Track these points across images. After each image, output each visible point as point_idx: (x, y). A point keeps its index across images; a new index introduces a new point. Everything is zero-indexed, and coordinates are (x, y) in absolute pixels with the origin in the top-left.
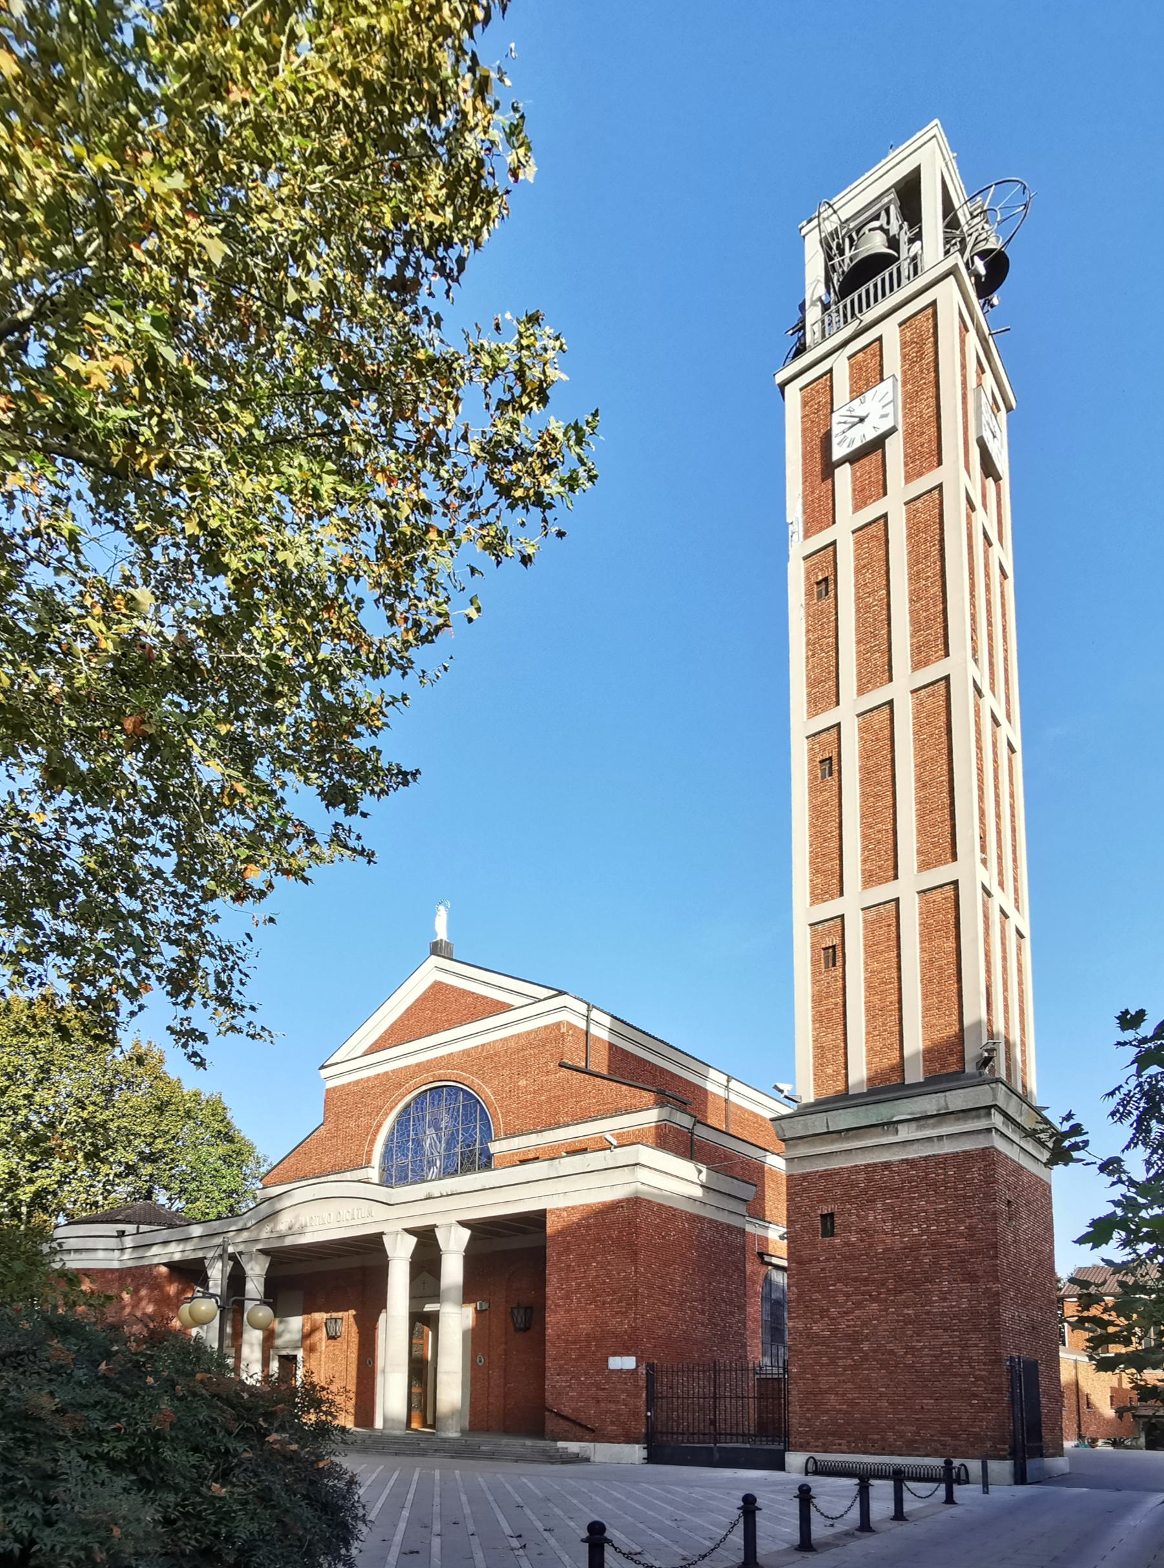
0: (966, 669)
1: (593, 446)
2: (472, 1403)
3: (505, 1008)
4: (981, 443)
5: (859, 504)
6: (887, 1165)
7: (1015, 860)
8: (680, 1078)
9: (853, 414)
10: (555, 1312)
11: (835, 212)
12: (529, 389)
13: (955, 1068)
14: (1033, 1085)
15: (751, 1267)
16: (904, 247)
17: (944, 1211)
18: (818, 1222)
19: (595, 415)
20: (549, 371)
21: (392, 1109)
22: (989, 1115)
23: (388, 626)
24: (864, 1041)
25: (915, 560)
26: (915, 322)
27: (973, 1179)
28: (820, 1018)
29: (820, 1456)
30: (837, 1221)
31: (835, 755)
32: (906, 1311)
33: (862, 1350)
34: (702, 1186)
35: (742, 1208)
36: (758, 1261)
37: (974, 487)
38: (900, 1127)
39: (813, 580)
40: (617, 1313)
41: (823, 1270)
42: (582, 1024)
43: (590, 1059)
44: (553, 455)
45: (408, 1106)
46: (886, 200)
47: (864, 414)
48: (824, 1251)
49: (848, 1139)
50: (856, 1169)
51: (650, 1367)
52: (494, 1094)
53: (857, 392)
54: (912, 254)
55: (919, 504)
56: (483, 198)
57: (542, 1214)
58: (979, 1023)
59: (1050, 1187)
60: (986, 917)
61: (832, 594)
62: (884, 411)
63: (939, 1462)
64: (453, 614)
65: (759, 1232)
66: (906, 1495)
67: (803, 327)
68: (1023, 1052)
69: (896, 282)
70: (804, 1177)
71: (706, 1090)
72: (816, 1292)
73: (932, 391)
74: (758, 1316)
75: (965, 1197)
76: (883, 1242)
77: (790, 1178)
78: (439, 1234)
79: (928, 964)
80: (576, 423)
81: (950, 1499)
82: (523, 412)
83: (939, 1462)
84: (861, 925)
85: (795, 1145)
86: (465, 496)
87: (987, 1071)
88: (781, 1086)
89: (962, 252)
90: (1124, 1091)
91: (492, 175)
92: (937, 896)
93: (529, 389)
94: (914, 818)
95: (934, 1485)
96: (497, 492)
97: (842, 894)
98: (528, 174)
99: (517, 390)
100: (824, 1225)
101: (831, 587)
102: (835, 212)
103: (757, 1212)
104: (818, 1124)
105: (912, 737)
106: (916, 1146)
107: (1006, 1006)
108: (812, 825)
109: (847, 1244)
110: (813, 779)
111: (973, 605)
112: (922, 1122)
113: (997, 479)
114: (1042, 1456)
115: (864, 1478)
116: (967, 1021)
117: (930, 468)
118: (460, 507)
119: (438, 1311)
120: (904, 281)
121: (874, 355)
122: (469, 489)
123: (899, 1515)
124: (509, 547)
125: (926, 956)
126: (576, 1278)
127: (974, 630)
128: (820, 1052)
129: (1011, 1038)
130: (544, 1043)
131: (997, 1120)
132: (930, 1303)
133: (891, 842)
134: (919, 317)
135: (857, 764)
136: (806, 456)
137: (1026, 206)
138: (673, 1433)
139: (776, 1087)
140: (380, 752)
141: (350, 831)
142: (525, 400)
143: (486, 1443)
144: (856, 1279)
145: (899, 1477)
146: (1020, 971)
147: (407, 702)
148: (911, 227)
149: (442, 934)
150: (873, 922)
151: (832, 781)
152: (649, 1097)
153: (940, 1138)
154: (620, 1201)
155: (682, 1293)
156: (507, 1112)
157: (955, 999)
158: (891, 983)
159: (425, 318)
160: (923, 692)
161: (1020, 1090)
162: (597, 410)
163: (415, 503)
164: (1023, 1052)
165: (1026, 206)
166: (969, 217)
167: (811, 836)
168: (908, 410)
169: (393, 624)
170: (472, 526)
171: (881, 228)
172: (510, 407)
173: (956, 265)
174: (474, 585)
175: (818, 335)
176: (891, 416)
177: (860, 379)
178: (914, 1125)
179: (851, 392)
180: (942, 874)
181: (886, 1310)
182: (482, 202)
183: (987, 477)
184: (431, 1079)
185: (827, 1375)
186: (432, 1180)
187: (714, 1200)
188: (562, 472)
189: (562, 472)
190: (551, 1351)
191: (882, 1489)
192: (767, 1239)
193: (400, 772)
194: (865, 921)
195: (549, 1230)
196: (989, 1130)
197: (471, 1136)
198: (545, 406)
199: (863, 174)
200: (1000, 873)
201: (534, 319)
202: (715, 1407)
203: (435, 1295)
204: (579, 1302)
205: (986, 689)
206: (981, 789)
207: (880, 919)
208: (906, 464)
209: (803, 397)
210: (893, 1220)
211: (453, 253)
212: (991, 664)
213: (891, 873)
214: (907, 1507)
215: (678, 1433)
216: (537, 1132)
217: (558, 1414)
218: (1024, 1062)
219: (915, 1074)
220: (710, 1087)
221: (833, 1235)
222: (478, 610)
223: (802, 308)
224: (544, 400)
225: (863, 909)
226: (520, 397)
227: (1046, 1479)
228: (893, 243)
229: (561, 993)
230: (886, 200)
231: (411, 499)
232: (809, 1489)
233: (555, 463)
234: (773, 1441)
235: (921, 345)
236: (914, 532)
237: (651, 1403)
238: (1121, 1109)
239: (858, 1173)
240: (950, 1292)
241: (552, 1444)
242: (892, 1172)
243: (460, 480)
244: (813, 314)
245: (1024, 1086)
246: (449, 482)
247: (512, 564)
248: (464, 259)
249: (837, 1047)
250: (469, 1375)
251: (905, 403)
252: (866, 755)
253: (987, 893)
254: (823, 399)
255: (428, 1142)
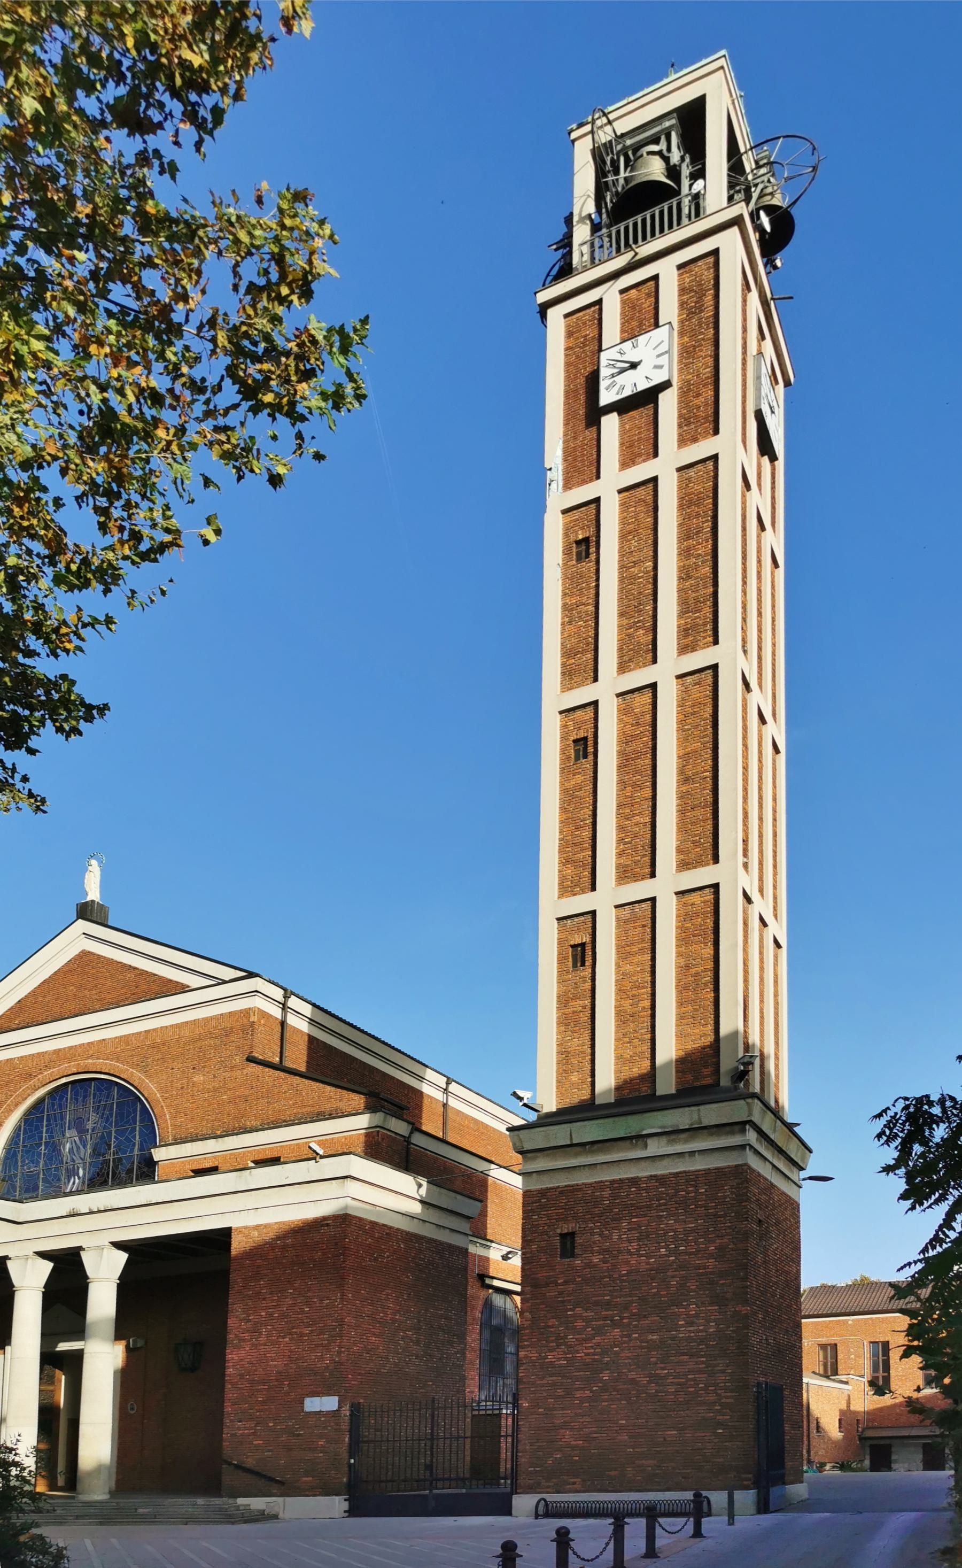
0: (735, 659)
1: (360, 361)
2: (118, 1457)
3: (183, 989)
4: (759, 416)
5: (627, 461)
6: (634, 1181)
7: (775, 866)
8: (393, 1078)
9: (624, 358)
10: (238, 1347)
11: (610, 122)
12: (290, 278)
13: (708, 1081)
14: (785, 1100)
15: (473, 1289)
16: (685, 183)
17: (693, 1230)
18: (557, 1241)
19: (365, 321)
20: (316, 262)
21: (17, 1105)
22: (743, 1131)
23: (99, 534)
24: (613, 1047)
25: (686, 534)
26: (695, 268)
27: (725, 1197)
28: (566, 1021)
29: (551, 1498)
30: (579, 1240)
31: (591, 736)
32: (650, 1337)
33: (601, 1380)
34: (421, 1202)
35: (465, 1226)
36: (478, 1284)
37: (751, 465)
38: (650, 1141)
39: (573, 538)
40: (317, 1346)
41: (561, 1293)
42: (277, 1012)
43: (286, 1053)
44: (312, 361)
45: (40, 1101)
46: (667, 124)
47: (636, 360)
48: (562, 1273)
49: (592, 1152)
50: (600, 1185)
51: (356, 1410)
52: (161, 1090)
53: (630, 333)
54: (694, 191)
55: (692, 472)
56: (242, 40)
57: (226, 1233)
58: (736, 1033)
59: (798, 1205)
60: (745, 924)
61: (593, 557)
62: (660, 361)
63: (689, 1495)
64: (185, 532)
65: (480, 1251)
66: (658, 1531)
67: (570, 245)
68: (777, 1066)
69: (675, 221)
70: (543, 1193)
71: (421, 1093)
72: (553, 1317)
73: (710, 350)
74: (475, 1345)
75: (716, 1216)
76: (627, 1263)
77: (527, 1194)
78: (86, 1257)
79: (684, 969)
80: (342, 327)
81: (698, 1533)
82: (281, 304)
83: (689, 1495)
84: (614, 923)
85: (534, 1159)
86: (197, 387)
87: (742, 1085)
88: (521, 1093)
89: (748, 200)
90: (891, 1113)
91: (259, 18)
92: (696, 898)
93: (290, 278)
94: (675, 814)
95: (683, 1520)
96: (239, 392)
97: (593, 888)
98: (305, 27)
99: (274, 276)
100: (563, 1245)
101: (593, 550)
102: (610, 122)
103: (480, 1233)
104: (560, 1135)
105: (675, 726)
106: (666, 1162)
107: (762, 1017)
108: (563, 810)
109: (590, 1265)
110: (565, 759)
111: (744, 592)
112: (673, 1137)
113: (773, 458)
114: (784, 1483)
115: (619, 1517)
116: (724, 1030)
117: (706, 435)
118: (194, 401)
119: (83, 1350)
120: (685, 220)
121: (648, 295)
122: (203, 380)
123: (651, 1552)
124: (255, 462)
125: (683, 961)
126: (267, 1308)
127: (744, 620)
128: (565, 1056)
129: (766, 1051)
130: (228, 1032)
131: (751, 1136)
132: (676, 1328)
133: (649, 836)
134: (700, 263)
135: (615, 748)
136: (569, 394)
137: (815, 169)
138: (382, 1482)
139: (515, 1094)
140: (73, 683)
141: (14, 770)
142: (285, 291)
143: (143, 1505)
144: (597, 1303)
145: (652, 1513)
146: (776, 982)
147: (113, 627)
148: (693, 162)
149: (93, 894)
150: (626, 921)
151: (587, 764)
152: (358, 1100)
153: (692, 1153)
154: (325, 1218)
155: (394, 1321)
156: (178, 1112)
157: (711, 1009)
158: (644, 987)
159: (156, 163)
160: (689, 679)
161: (772, 1104)
162: (367, 317)
163: (142, 390)
164: (777, 1066)
165: (815, 169)
166: (754, 166)
167: (561, 822)
168: (685, 365)
169: (105, 533)
170: (207, 426)
171: (660, 153)
172: (265, 296)
173: (741, 215)
174: (207, 500)
175: (586, 257)
176: (666, 368)
177: (632, 318)
178: (664, 1140)
179: (623, 331)
180: (703, 876)
181: (629, 1336)
182: (241, 44)
183: (763, 455)
184: (74, 1070)
185: (563, 1409)
186: (71, 1194)
187: (434, 1216)
188: (324, 381)
189: (324, 381)
190: (230, 1394)
191: (636, 1528)
192: (487, 1259)
193: (83, 703)
194: (618, 919)
195: (234, 1252)
196: (742, 1147)
197: (128, 1140)
198: (308, 302)
199: (642, 89)
200: (761, 879)
201: (300, 197)
202: (432, 1448)
203: (79, 1330)
204: (269, 1334)
205: (754, 684)
206: (745, 789)
207: (633, 919)
208: (680, 426)
209: (568, 326)
210: (639, 1239)
211: (209, 101)
212: (760, 658)
213: (648, 870)
214: (659, 1543)
215: (387, 1481)
216: (216, 1137)
217: (238, 1467)
218: (777, 1076)
219: (666, 1085)
220: (426, 1089)
221: (573, 1255)
222: (218, 532)
223: (569, 220)
224: (307, 294)
225: (616, 907)
226: (278, 284)
227: (786, 1506)
228: (673, 172)
229: (251, 975)
230: (667, 124)
231: (138, 385)
232: (568, 1532)
233: (313, 370)
234: (485, 1484)
235: (701, 296)
236: (686, 502)
237: (354, 1449)
238: (888, 1132)
239: (602, 1189)
240: (697, 1316)
241: (231, 1501)
242: (639, 1189)
243: (191, 367)
244: (581, 233)
245: (777, 1101)
246: (177, 367)
247: (257, 481)
248: (223, 111)
249: (582, 1052)
250: (117, 1424)
251: (681, 355)
252: (625, 740)
253: (748, 899)
254: (591, 333)
255: (68, 1146)
